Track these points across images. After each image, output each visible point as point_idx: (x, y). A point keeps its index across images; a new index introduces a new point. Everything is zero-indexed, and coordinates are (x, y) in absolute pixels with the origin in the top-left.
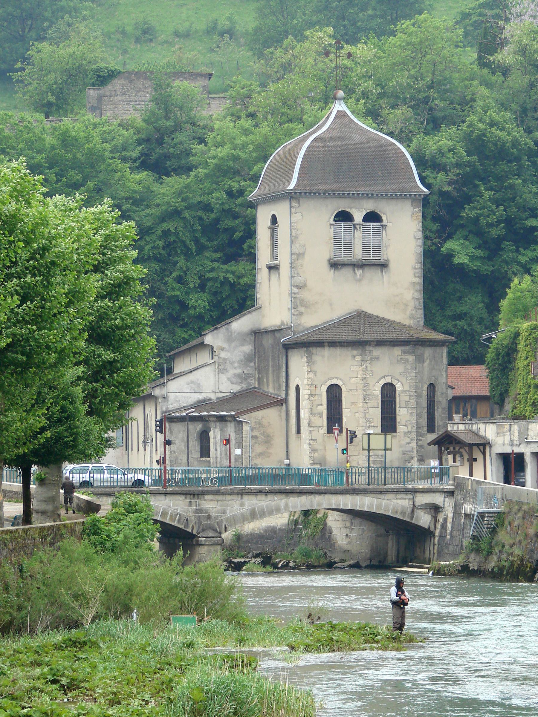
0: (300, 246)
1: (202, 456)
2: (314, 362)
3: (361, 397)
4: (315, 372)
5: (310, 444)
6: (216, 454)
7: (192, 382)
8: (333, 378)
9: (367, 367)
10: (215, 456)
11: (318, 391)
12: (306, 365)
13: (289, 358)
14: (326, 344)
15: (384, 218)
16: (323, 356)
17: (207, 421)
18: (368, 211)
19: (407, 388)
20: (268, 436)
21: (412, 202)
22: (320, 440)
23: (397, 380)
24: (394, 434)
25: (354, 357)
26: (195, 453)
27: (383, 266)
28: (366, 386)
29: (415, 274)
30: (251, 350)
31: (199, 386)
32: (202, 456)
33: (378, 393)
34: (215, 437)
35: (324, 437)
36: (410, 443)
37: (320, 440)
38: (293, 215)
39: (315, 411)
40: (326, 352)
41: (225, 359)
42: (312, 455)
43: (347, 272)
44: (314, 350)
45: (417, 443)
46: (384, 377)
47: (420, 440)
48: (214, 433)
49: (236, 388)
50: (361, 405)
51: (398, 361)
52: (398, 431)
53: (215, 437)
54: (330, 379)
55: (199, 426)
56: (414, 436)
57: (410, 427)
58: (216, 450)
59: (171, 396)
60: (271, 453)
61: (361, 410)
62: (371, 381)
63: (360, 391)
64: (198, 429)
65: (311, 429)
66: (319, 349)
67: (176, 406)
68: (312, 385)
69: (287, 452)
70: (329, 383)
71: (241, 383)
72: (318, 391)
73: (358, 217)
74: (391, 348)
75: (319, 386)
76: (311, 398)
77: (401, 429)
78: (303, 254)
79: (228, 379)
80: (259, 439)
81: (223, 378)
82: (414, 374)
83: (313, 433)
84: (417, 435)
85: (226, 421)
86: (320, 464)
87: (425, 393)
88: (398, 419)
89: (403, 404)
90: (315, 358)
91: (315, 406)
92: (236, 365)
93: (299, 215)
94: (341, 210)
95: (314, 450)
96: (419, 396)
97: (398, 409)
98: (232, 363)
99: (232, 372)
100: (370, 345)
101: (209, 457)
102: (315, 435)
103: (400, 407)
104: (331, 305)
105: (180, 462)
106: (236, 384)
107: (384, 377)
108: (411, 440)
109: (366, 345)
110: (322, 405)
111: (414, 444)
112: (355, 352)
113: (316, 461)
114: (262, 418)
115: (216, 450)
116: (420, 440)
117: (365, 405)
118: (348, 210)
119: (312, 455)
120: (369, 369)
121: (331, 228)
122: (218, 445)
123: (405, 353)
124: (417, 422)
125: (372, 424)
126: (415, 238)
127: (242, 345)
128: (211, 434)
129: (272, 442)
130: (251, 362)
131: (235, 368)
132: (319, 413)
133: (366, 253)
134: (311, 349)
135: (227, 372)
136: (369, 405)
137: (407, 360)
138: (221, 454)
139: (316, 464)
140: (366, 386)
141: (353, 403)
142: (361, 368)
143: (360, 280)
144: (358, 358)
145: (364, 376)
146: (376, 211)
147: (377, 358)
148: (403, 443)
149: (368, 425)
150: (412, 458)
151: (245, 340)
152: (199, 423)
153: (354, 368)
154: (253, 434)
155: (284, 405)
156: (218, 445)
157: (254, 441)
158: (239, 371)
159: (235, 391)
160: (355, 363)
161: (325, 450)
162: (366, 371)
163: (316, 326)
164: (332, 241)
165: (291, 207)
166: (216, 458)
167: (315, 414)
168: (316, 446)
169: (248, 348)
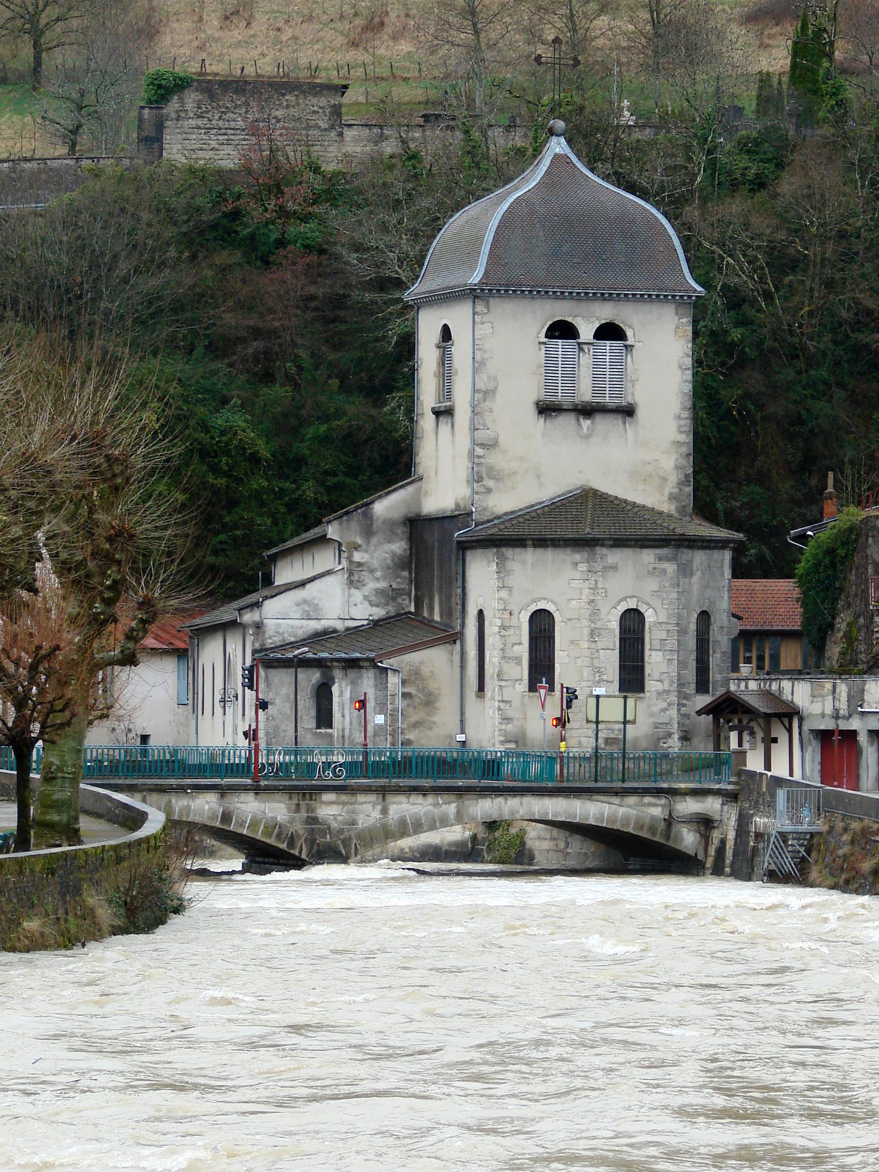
0: (489, 377)
1: (318, 727)
2: (509, 573)
3: (586, 632)
4: (510, 589)
5: (499, 709)
6: (343, 722)
7: (305, 601)
8: (540, 599)
9: (596, 581)
10: (340, 727)
11: (514, 621)
12: (495, 576)
13: (467, 565)
14: (529, 542)
15: (629, 333)
16: (524, 563)
17: (328, 667)
18: (603, 322)
19: (663, 618)
20: (430, 694)
21: (676, 308)
22: (516, 702)
23: (647, 604)
24: (642, 695)
25: (576, 564)
26: (308, 720)
27: (628, 412)
28: (595, 614)
29: (680, 426)
30: (405, 550)
31: (316, 608)
32: (318, 727)
33: (615, 625)
34: (341, 694)
35: (523, 697)
36: (667, 709)
37: (516, 702)
38: (477, 326)
39: (509, 653)
40: (530, 555)
41: (360, 564)
42: (503, 727)
43: (567, 421)
44: (509, 552)
45: (679, 710)
46: (625, 599)
47: (684, 705)
48: (340, 687)
49: (379, 613)
50: (586, 645)
51: (649, 572)
52: (646, 689)
53: (341, 694)
54: (534, 601)
55: (315, 676)
56: (673, 698)
57: (666, 683)
58: (343, 716)
59: (270, 625)
60: (434, 723)
61: (587, 653)
62: (604, 606)
63: (585, 622)
64: (314, 681)
65: (503, 683)
66: (517, 550)
67: (277, 640)
68: (505, 610)
69: (462, 721)
70: (534, 608)
71: (386, 605)
72: (514, 621)
73: (586, 331)
74: (638, 550)
75: (515, 613)
76: (503, 633)
77: (651, 685)
78: (494, 391)
79: (365, 597)
80: (417, 700)
81: (357, 595)
82: (675, 596)
83: (505, 690)
84: (679, 697)
85: (361, 667)
86: (516, 742)
87: (693, 627)
88: (648, 670)
89: (656, 644)
90: (509, 565)
91: (509, 646)
92: (378, 574)
93: (487, 326)
94: (557, 319)
95: (507, 720)
96: (683, 632)
97: (647, 653)
98: (372, 571)
99: (372, 585)
100: (603, 545)
101: (331, 727)
102: (508, 694)
103: (651, 650)
104: (538, 477)
105: (282, 734)
106: (377, 606)
107: (625, 599)
108: (669, 705)
109: (595, 545)
110: (520, 644)
111: (673, 713)
112: (577, 557)
113: (509, 738)
114: (421, 663)
115: (343, 716)
116: (684, 705)
117: (593, 645)
118: (570, 320)
119: (503, 727)
120: (600, 585)
121: (540, 349)
122: (347, 707)
123: (660, 559)
124: (679, 674)
125: (605, 677)
126: (680, 368)
127: (390, 541)
128: (335, 689)
129: (437, 704)
130: (403, 569)
131: (377, 579)
132: (516, 658)
133: (597, 390)
134: (504, 550)
135: (364, 585)
136: (600, 645)
137: (664, 571)
138: (351, 723)
139: (510, 741)
140: (595, 614)
141: (572, 642)
142: (587, 584)
143: (587, 437)
144: (583, 567)
145: (592, 597)
146: (616, 322)
147: (614, 568)
148: (656, 709)
149: (597, 678)
150: (670, 735)
151: (394, 533)
152: (315, 670)
153: (576, 584)
154: (406, 690)
155: (458, 642)
156: (347, 707)
157: (406, 702)
158: (383, 585)
159: (376, 618)
160: (578, 575)
161: (525, 718)
162: (594, 589)
163: (512, 512)
164: (543, 370)
165: (474, 314)
166: (343, 730)
167: (510, 658)
168: (510, 713)
169: (399, 547)
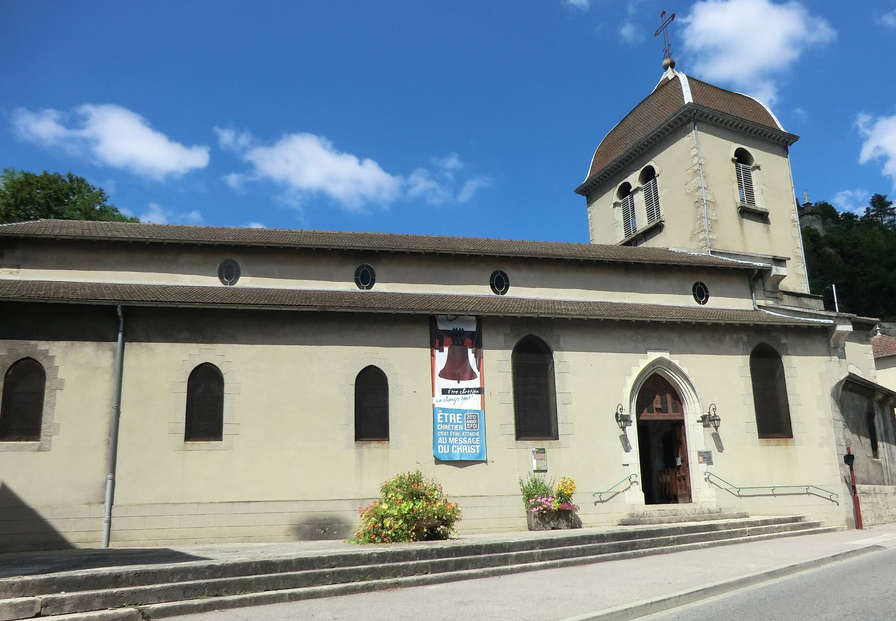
128: (876, 420)
